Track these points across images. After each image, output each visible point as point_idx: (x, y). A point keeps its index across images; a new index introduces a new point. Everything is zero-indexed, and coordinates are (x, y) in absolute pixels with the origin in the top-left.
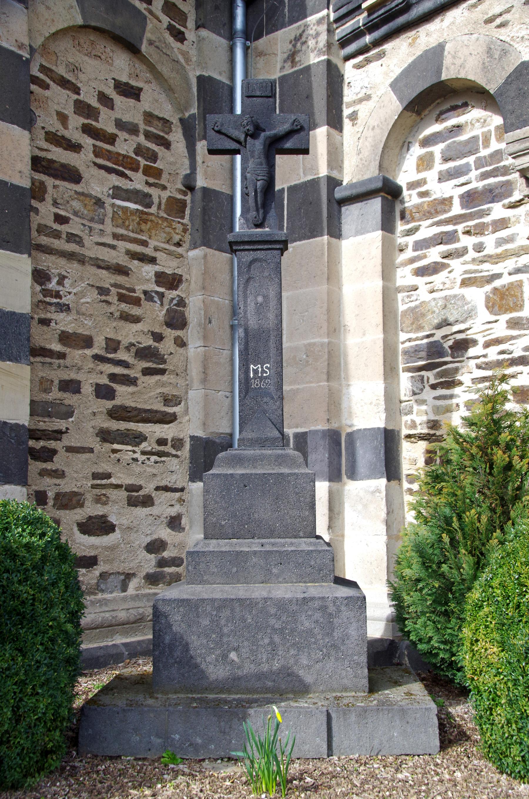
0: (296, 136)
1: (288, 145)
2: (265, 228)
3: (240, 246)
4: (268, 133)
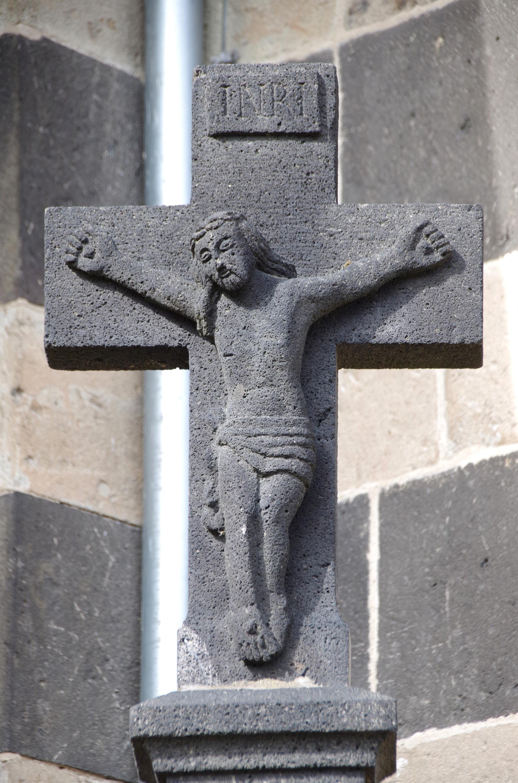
0: (425, 294)
1: (393, 327)
2: (292, 674)
3: (184, 755)
4: (305, 282)
